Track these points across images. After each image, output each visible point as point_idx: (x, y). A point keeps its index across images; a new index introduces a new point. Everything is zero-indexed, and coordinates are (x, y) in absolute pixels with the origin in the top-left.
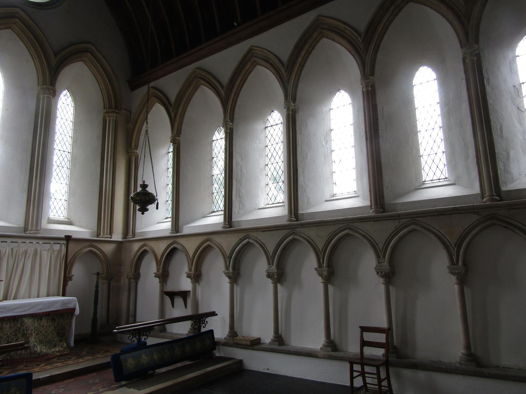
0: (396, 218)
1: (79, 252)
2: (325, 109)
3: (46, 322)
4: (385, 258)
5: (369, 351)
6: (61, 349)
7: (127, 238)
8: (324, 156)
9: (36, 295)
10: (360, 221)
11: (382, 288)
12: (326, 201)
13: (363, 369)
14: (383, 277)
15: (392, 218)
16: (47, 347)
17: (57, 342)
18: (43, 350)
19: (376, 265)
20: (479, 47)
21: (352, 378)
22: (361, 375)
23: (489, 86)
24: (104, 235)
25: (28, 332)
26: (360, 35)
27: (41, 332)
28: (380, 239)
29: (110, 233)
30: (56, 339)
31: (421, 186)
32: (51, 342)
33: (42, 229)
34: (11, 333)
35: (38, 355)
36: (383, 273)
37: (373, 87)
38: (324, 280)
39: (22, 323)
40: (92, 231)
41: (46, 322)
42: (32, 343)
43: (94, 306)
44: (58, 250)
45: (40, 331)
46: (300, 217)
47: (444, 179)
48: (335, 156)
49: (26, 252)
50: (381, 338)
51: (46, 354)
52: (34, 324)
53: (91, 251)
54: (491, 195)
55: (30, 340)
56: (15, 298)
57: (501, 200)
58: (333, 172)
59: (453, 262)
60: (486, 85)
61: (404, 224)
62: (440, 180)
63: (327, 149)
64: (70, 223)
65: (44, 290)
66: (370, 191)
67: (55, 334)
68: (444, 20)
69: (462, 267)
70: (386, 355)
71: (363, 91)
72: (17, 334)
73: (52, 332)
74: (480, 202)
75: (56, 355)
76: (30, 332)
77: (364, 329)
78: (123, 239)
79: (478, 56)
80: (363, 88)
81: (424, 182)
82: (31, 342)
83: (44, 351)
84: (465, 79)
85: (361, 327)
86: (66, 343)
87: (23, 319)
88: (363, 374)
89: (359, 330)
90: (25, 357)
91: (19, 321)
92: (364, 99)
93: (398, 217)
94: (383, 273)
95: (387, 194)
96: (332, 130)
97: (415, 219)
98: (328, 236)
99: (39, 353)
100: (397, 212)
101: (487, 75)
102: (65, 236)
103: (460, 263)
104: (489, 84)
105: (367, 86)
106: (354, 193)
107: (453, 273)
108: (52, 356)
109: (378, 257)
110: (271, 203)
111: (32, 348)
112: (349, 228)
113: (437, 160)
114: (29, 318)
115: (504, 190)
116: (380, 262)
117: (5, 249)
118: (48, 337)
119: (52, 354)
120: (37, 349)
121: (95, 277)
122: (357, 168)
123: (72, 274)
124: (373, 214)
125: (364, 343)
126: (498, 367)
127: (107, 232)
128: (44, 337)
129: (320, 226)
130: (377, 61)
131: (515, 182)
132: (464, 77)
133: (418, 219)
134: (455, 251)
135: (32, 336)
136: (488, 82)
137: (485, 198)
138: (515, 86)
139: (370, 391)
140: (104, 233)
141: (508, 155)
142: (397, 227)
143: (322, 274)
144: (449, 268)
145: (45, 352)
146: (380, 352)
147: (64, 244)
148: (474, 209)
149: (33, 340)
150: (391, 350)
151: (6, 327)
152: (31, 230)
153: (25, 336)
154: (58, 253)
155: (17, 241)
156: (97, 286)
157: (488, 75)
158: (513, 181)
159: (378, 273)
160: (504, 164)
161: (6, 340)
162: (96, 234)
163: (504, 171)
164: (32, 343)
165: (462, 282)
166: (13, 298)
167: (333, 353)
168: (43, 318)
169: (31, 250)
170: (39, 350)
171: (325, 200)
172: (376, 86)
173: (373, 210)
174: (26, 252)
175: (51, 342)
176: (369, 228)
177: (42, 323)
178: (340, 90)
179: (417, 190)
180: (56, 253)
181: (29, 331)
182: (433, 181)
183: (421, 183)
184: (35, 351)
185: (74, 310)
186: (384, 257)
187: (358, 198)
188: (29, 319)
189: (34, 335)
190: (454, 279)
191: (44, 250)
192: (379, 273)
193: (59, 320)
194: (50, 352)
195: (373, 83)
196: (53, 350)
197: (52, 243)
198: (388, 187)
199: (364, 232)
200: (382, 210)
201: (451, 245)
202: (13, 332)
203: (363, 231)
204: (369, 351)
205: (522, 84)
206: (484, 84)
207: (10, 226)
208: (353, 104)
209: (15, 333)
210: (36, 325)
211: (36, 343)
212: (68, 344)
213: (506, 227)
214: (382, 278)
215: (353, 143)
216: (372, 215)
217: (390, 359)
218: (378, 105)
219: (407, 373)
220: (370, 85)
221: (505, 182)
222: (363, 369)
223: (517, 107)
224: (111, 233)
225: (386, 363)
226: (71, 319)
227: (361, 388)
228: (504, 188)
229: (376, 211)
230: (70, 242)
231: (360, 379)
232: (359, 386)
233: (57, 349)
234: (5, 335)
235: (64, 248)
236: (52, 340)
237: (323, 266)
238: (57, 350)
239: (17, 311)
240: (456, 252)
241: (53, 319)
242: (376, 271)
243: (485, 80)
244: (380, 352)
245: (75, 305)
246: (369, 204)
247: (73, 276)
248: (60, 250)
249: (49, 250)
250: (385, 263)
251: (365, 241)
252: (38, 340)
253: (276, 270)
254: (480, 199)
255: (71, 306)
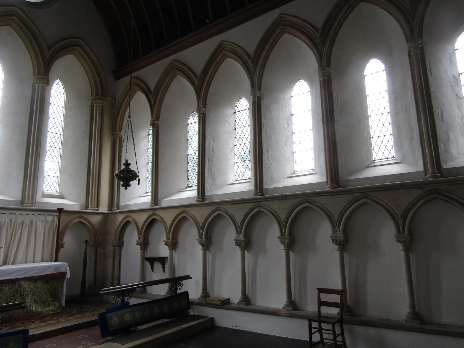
0: (350, 192)
1: (70, 223)
2: (287, 96)
3: (41, 285)
4: (340, 228)
5: (325, 310)
6: (54, 308)
7: (112, 211)
8: (286, 138)
9: (32, 260)
10: (317, 195)
11: (337, 254)
12: (288, 177)
13: (320, 326)
14: (337, 244)
15: (346, 192)
16: (42, 306)
17: (50, 302)
18: (38, 309)
19: (332, 234)
20: (422, 41)
21: (311, 334)
22: (319, 331)
23: (432, 76)
24: (92, 208)
25: (25, 294)
26: (317, 31)
27: (36, 293)
28: (336, 211)
29: (97, 206)
30: (49, 299)
31: (371, 164)
32: (45, 302)
33: (37, 202)
34: (10, 294)
35: (34, 314)
36: (338, 241)
37: (329, 76)
38: (286, 248)
39: (20, 286)
40: (81, 204)
41: (40, 284)
42: (28, 303)
43: (83, 270)
44: (51, 221)
45: (35, 292)
46: (265, 192)
47: (392, 158)
48: (295, 138)
49: (23, 222)
50: (336, 298)
51: (41, 313)
52: (30, 287)
53: (80, 222)
54: (433, 173)
55: (27, 300)
56: (13, 263)
57: (442, 177)
58: (294, 152)
59: (400, 232)
60: (429, 75)
61: (356, 198)
62: (388, 159)
63: (288, 131)
64: (62, 197)
65: (39, 256)
66: (327, 169)
67: (49, 295)
68: (391, 17)
69: (408, 236)
70: (341, 313)
71: (320, 81)
72: (15, 295)
73: (46, 293)
74: (423, 179)
75: (49, 313)
76: (26, 293)
77: (321, 291)
78: (108, 211)
79: (422, 49)
80: (320, 78)
81: (374, 160)
82: (27, 302)
83: (39, 310)
84: (410, 70)
85: (318, 289)
86: (58, 303)
87: (21, 281)
88: (320, 330)
89: (317, 292)
90: (22, 315)
91: (17, 284)
92: (321, 88)
93: (351, 192)
94: (338, 241)
95: (341, 171)
96: (293, 115)
97: (367, 193)
98: (289, 208)
99: (34, 312)
100: (350, 187)
101: (429, 66)
102: (57, 208)
103: (406, 232)
104: (431, 74)
105: (324, 76)
106: (313, 170)
107: (399, 241)
108: (46, 315)
109: (334, 227)
110: (239, 179)
111: (28, 307)
112: (308, 202)
113: (385, 142)
114: (25, 281)
115: (444, 168)
116: (335, 231)
117: (4, 220)
118: (43, 298)
119: (46, 312)
120: (33, 308)
121: (84, 245)
122: (315, 148)
123: (64, 242)
124: (329, 189)
125: (321, 303)
126: (439, 324)
127: (94, 205)
128: (38, 297)
129: (282, 199)
130: (332, 54)
131: (454, 161)
132: (409, 68)
133: (369, 193)
134: (401, 222)
135: (28, 296)
136: (430, 73)
137: (428, 175)
138: (454, 76)
139: (327, 345)
140: (92, 206)
141: (448, 137)
142: (350, 201)
143: (284, 242)
144: (396, 236)
145: (40, 311)
146: (335, 311)
147: (56, 215)
148: (418, 185)
149: (29, 300)
150: (345, 309)
151: (5, 288)
152: (27, 204)
153: (22, 296)
154: (51, 224)
155: (15, 213)
156: (86, 253)
157: (431, 66)
158: (452, 160)
159: (333, 241)
160: (445, 145)
161: (5, 300)
162: (85, 206)
163: (445, 151)
164: (28, 303)
165: (408, 249)
166: (12, 263)
167: (294, 312)
168: (38, 281)
169: (27, 221)
170: (34, 309)
171: (286, 177)
172: (332, 76)
173: (329, 185)
174: (23, 222)
175: (45, 302)
176: (325, 201)
177: (37, 286)
178: (300, 79)
179: (368, 168)
180: (49, 223)
181: (26, 292)
182: (382, 160)
183: (371, 162)
184: (31, 310)
185: (65, 273)
186: (339, 227)
187: (316, 175)
188: (25, 282)
189: (30, 296)
190: (400, 246)
191: (39, 221)
192: (335, 241)
193: (52, 282)
194: (44, 311)
195: (329, 74)
196: (47, 309)
197: (46, 215)
198: (342, 165)
199: (321, 205)
200: (337, 186)
201: (398, 216)
202: (12, 293)
203: (320, 204)
204: (325, 310)
205: (460, 74)
206: (427, 74)
207: (9, 199)
208: (312, 92)
209: (14, 294)
210: (32, 287)
211: (31, 303)
212: (60, 304)
213: (446, 201)
214: (337, 246)
215: (311, 127)
216: (328, 190)
217: (344, 317)
218: (333, 93)
219: (359, 329)
220: (326, 75)
221: (446, 161)
222: (320, 326)
223: (456, 95)
224: (98, 206)
225: (341, 321)
226: (63, 282)
227: (318, 342)
228: (445, 166)
229: (332, 187)
230: (61, 213)
231: (318, 334)
232: (316, 341)
233: (50, 309)
234: (4, 296)
235: (56, 219)
236: (46, 301)
237: (285, 235)
238: (50, 309)
239: (15, 274)
240: (402, 223)
241: (47, 282)
242: (332, 240)
243: (428, 70)
244: (335, 311)
245: (66, 270)
246: (326, 180)
247: (64, 243)
248: (53, 221)
249: (43, 221)
250: (340, 232)
251: (322, 212)
252: (34, 300)
253: (244, 238)
254: (423, 175)
255: (62, 270)
